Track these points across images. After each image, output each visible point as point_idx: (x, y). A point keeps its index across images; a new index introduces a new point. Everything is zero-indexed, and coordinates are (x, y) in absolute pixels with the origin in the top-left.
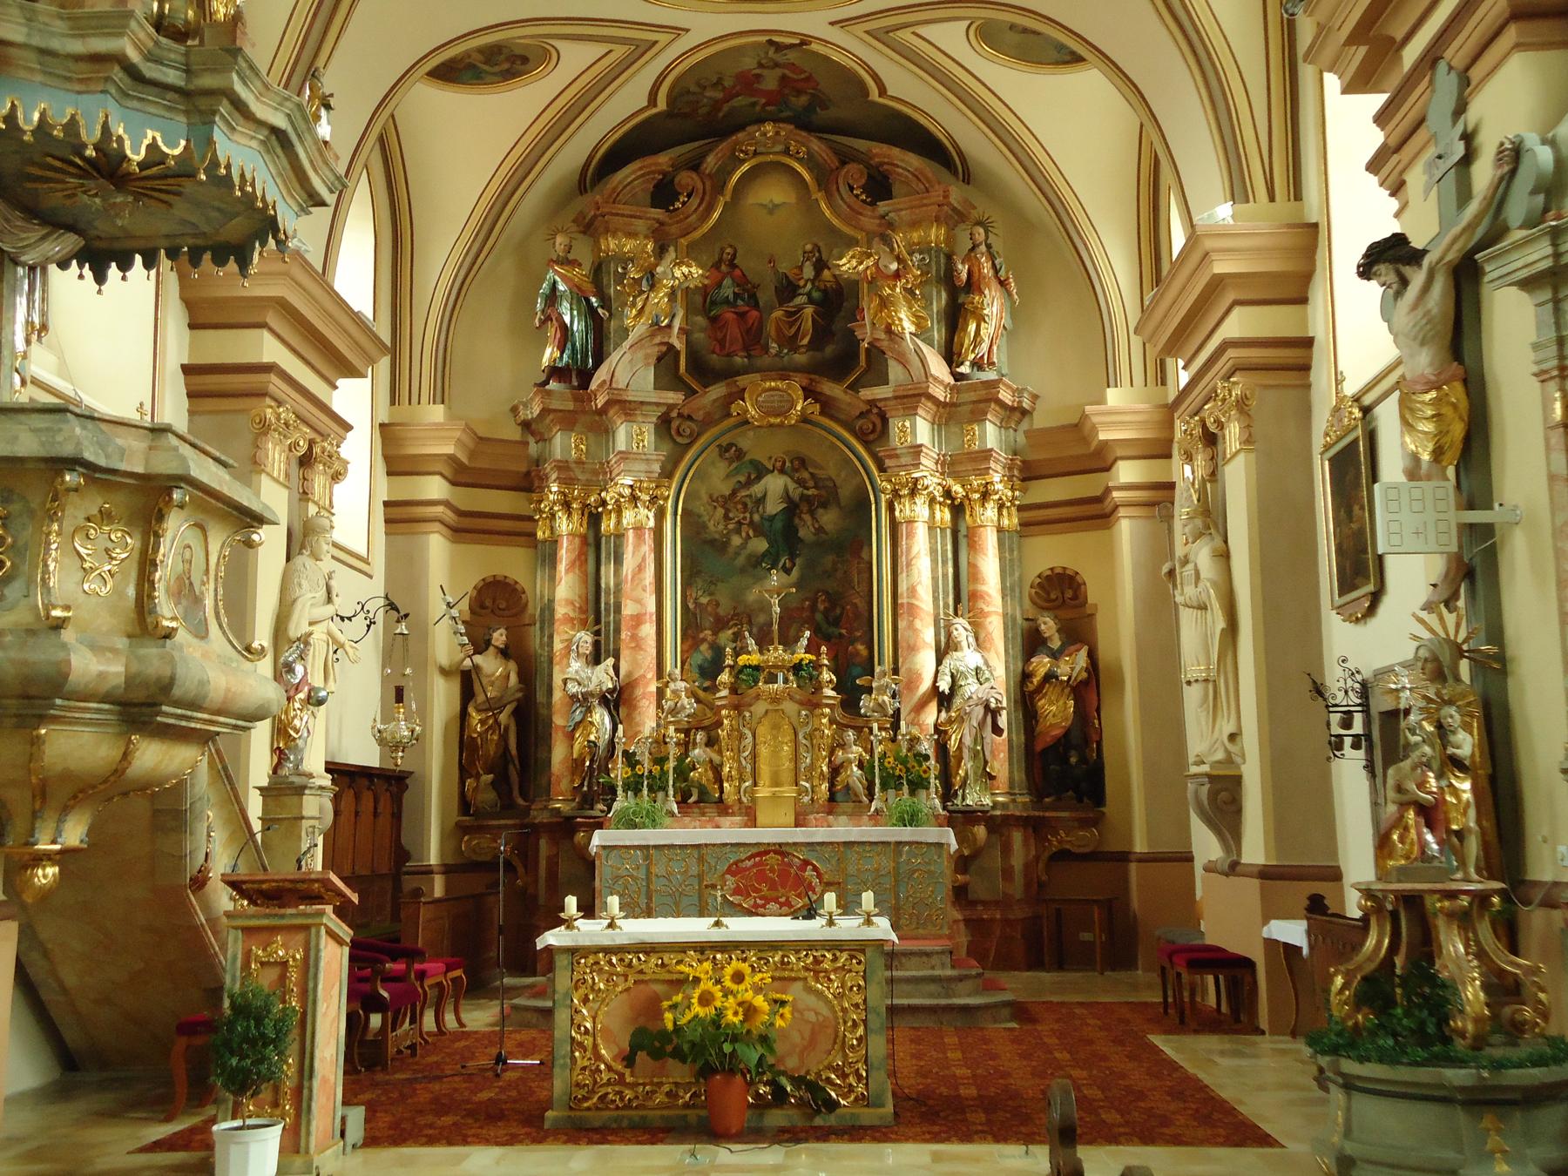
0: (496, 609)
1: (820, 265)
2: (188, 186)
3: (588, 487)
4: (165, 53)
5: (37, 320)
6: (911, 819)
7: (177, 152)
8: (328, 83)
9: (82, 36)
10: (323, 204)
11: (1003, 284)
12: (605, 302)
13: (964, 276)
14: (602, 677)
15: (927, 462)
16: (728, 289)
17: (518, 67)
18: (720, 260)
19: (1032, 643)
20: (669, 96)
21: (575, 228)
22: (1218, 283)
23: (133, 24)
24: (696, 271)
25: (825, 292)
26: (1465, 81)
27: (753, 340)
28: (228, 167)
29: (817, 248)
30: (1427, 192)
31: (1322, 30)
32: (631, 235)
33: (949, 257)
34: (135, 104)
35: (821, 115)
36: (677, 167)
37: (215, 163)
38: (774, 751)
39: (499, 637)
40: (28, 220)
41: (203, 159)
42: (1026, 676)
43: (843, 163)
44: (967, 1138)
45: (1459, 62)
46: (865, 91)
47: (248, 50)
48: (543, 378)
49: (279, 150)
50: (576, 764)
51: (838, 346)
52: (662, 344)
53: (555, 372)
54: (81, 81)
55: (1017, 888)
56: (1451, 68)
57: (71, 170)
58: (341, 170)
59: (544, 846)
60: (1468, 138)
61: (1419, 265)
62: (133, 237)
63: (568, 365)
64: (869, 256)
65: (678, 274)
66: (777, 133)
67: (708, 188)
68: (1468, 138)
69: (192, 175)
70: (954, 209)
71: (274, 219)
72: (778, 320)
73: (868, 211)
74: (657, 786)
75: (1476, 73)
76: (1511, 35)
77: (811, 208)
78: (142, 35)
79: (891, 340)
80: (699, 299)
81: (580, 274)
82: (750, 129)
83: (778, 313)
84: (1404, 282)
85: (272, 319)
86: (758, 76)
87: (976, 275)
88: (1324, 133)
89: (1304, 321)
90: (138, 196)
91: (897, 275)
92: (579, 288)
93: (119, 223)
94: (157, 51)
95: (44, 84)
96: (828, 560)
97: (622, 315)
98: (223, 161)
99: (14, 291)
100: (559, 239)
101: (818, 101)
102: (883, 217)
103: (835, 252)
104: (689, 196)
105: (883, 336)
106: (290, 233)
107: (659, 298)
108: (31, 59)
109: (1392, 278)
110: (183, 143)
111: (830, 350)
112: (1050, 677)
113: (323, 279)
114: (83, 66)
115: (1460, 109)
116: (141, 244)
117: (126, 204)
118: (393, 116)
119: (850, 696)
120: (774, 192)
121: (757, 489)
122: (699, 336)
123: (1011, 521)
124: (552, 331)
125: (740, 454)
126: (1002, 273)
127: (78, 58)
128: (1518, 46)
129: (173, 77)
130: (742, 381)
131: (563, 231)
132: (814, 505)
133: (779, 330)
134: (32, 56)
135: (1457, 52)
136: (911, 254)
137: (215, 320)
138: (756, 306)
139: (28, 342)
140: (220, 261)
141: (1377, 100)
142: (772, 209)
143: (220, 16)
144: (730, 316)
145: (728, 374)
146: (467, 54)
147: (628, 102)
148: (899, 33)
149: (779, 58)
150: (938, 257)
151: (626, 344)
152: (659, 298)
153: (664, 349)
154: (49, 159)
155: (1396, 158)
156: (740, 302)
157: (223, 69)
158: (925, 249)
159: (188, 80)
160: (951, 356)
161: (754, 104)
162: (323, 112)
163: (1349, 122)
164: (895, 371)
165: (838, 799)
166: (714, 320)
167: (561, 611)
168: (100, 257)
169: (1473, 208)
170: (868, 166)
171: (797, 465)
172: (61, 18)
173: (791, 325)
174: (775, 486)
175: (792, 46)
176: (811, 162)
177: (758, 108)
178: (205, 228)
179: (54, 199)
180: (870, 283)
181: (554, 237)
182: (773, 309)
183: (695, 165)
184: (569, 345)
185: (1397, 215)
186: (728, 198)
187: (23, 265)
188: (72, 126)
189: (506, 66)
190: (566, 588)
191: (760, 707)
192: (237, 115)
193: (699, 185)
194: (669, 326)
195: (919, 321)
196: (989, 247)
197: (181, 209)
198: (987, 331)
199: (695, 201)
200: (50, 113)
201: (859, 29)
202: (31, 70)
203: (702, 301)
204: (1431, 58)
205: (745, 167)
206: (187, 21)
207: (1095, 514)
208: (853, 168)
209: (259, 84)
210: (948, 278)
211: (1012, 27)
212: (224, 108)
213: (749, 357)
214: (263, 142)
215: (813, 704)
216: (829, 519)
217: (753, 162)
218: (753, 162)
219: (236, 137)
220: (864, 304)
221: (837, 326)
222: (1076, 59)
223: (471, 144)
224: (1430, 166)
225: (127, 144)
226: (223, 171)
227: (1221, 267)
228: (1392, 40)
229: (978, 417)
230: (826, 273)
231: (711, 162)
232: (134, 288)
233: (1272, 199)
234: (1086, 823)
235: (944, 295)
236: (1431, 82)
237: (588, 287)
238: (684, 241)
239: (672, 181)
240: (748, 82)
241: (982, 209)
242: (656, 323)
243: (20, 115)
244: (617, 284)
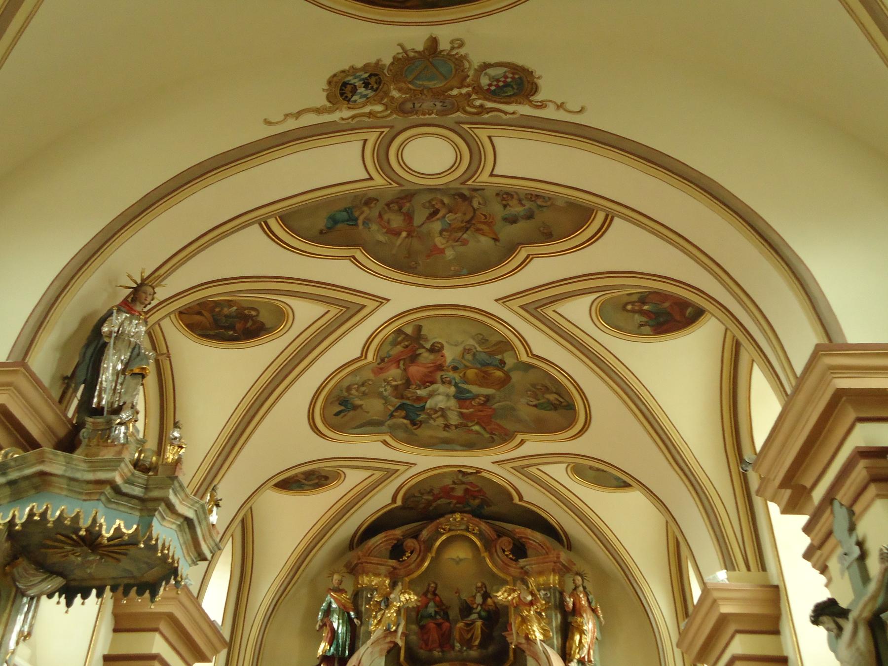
2: (132, 550)
4: (136, 479)
5: (26, 629)
7: (130, 532)
8: (219, 495)
9: (94, 471)
10: (205, 559)
11: (594, 611)
12: (359, 615)
13: (571, 605)
16: (432, 609)
17: (323, 482)
18: (428, 591)
20: (405, 494)
21: (344, 570)
22: (724, 619)
23: (123, 465)
24: (414, 597)
25: (488, 612)
26: (851, 513)
28: (157, 540)
29: (483, 584)
30: (842, 574)
31: (764, 481)
32: (377, 575)
33: (561, 594)
34: (113, 506)
35: (487, 510)
36: (406, 536)
37: (150, 538)
40: (37, 570)
41: (144, 536)
43: (499, 536)
45: (846, 501)
46: (511, 498)
47: (181, 478)
48: (318, 662)
49: (187, 530)
52: (391, 642)
54: (87, 494)
56: (841, 505)
57: (69, 541)
58: (218, 540)
60: (860, 544)
61: (847, 619)
62: (94, 579)
63: (333, 654)
64: (514, 591)
65: (402, 599)
66: (462, 519)
67: (422, 548)
68: (860, 544)
69: (136, 544)
70: (563, 565)
71: (176, 569)
72: (460, 629)
73: (513, 564)
75: (857, 508)
76: (872, 490)
77: (481, 562)
78: (126, 470)
79: (528, 644)
80: (414, 614)
81: (345, 597)
82: (447, 516)
83: (460, 625)
84: (840, 629)
85: (163, 626)
86: (453, 489)
87: (578, 605)
88: (773, 533)
89: (780, 646)
90: (102, 556)
91: (531, 603)
92: (345, 607)
93: (89, 571)
94: (133, 478)
95: (67, 496)
97: (368, 624)
98: (154, 536)
99: (18, 612)
100: (336, 577)
101: (485, 502)
102: (522, 568)
103: (495, 588)
104: (412, 553)
105: (523, 641)
106: (184, 576)
107: (391, 613)
108: (63, 483)
109: (832, 625)
110: (135, 526)
111: (491, 649)
113: (196, 600)
114: (91, 486)
115: (852, 528)
116: (97, 583)
117: (94, 561)
118: (251, 508)
120: (459, 552)
122: (413, 638)
124: (325, 633)
126: (593, 604)
127: (89, 482)
128: (879, 496)
129: (137, 491)
131: (338, 572)
133: (461, 635)
134: (64, 481)
135: (844, 495)
136: (539, 590)
137: (128, 626)
138: (448, 620)
139: (17, 643)
140: (140, 593)
141: (804, 519)
142: (458, 561)
143: (170, 460)
144: (432, 625)
146: (296, 475)
147: (381, 500)
148: (530, 469)
149: (464, 479)
150: (555, 593)
151: (369, 642)
152: (391, 613)
153: (392, 645)
154: (59, 537)
155: (819, 552)
156: (438, 617)
157: (164, 486)
158: (547, 588)
159: (145, 493)
161: (450, 503)
162: (215, 509)
163: (788, 532)
166: (422, 628)
168: (71, 591)
169: (872, 586)
170: (513, 539)
172: (85, 461)
173: (468, 631)
175: (471, 473)
176: (481, 535)
177: (452, 506)
178: (136, 573)
179: (54, 558)
180: (515, 607)
181: (332, 575)
182: (457, 622)
183: (415, 536)
184: (335, 642)
185: (827, 586)
186: (433, 555)
187: (27, 596)
188: (76, 519)
189: (316, 481)
192: (168, 511)
193: (417, 547)
194: (396, 631)
195: (545, 633)
196: (584, 588)
197: (125, 564)
198: (587, 639)
199: (415, 556)
200: (66, 511)
201: (508, 466)
202: (61, 488)
203: (415, 616)
204: (829, 499)
205: (444, 537)
206: (151, 463)
208: (505, 539)
209: (183, 495)
210: (561, 606)
211: (591, 468)
212: (162, 508)
213: (443, 651)
214: (179, 526)
217: (449, 534)
218: (449, 534)
219: (165, 523)
220: (512, 620)
221: (496, 634)
222: (626, 485)
223: (290, 523)
224: (841, 560)
225: (104, 527)
226: (154, 542)
227: (726, 609)
228: (804, 487)
230: (489, 601)
231: (425, 534)
232: (88, 608)
233: (749, 569)
235: (559, 616)
236: (832, 512)
237: (350, 605)
238: (407, 579)
239: (402, 544)
240: (447, 492)
241: (580, 565)
242: (388, 629)
243: (49, 512)
244: (366, 604)
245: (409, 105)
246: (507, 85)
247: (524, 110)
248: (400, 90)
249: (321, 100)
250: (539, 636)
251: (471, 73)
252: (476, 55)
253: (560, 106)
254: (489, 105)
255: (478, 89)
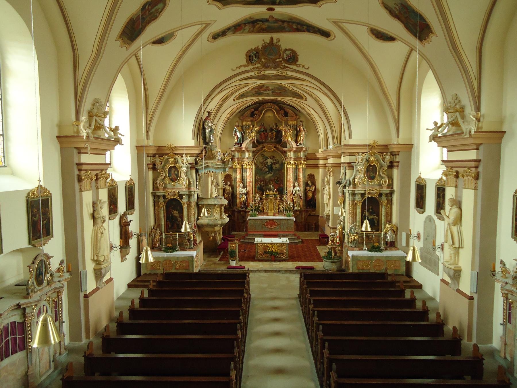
0: (228, 178)
1: (277, 126)
3: (242, 161)
6: (289, 216)
11: (305, 131)
12: (244, 133)
14: (244, 191)
15: (292, 159)
16: (262, 130)
19: (307, 185)
27: (266, 137)
38: (271, 206)
39: (229, 183)
42: (306, 190)
44: (295, 261)
50: (241, 203)
51: (279, 140)
53: (236, 143)
55: (303, 220)
59: (236, 214)
74: (255, 210)
96: (277, 172)
111: (278, 139)
112: (309, 190)
119: (281, 199)
120: (269, 114)
121: (267, 161)
123: (304, 166)
124: (236, 137)
125: (264, 156)
130: (265, 145)
132: (275, 164)
144: (262, 134)
145: (262, 143)
160: (296, 142)
164: (288, 145)
165: (279, 212)
166: (260, 134)
167: (238, 180)
171: (273, 158)
174: (269, 161)
176: (275, 109)
190: (238, 177)
191: (269, 200)
207: (316, 166)
215: (276, 199)
216: (277, 166)
229: (300, 152)
234: (313, 211)
245: (267, 65)
246: (291, 58)
247: (295, 67)
248: (264, 59)
249: (245, 63)
250: (290, 140)
251: (282, 53)
252: (284, 46)
253: (303, 66)
254: (286, 65)
255: (283, 59)
